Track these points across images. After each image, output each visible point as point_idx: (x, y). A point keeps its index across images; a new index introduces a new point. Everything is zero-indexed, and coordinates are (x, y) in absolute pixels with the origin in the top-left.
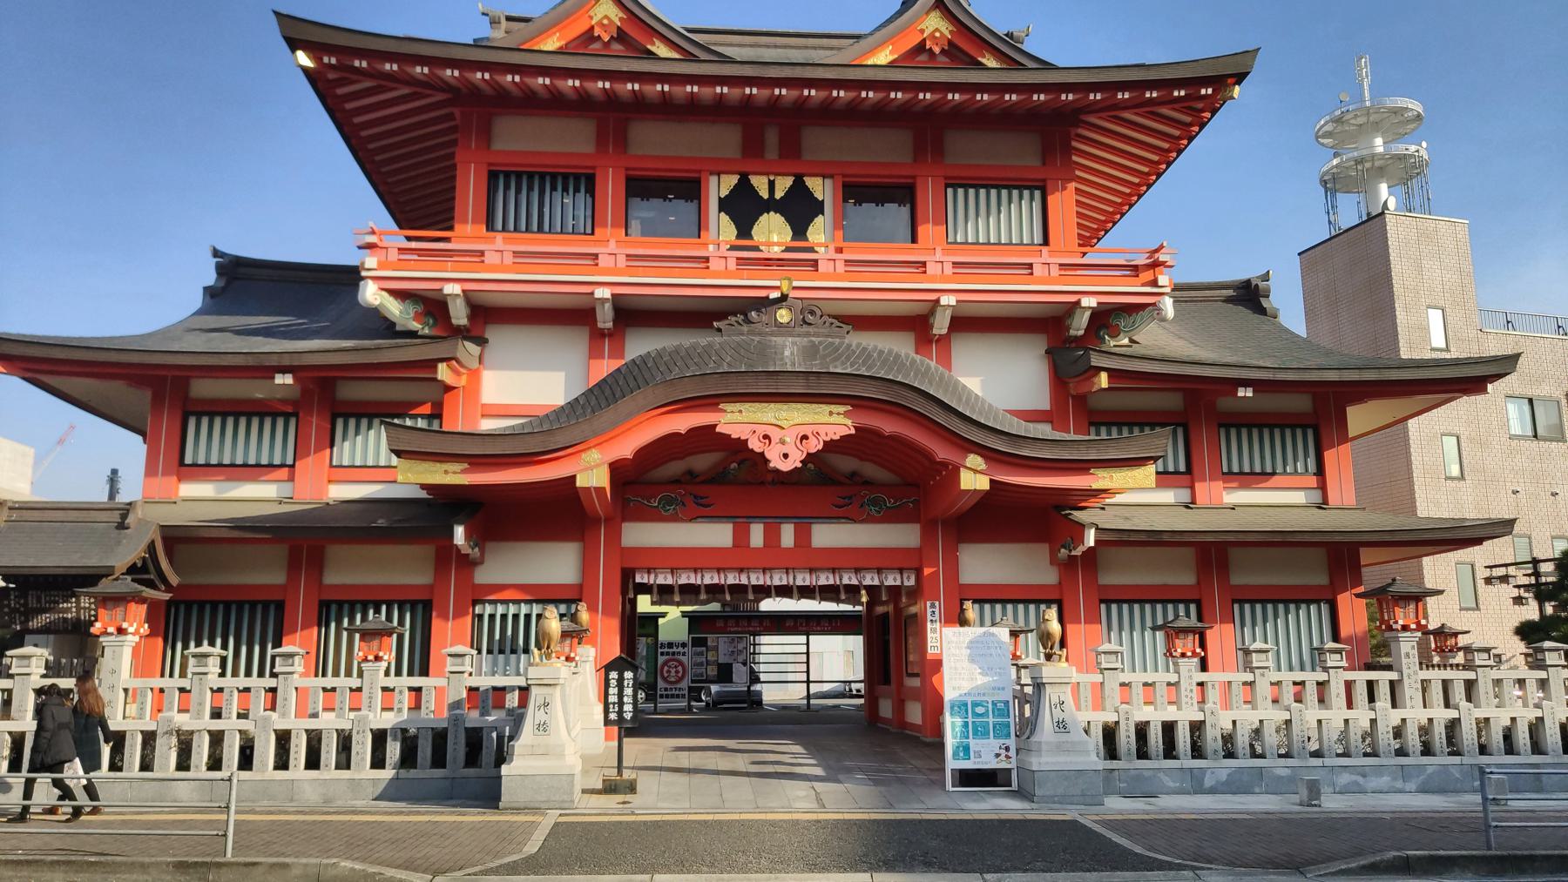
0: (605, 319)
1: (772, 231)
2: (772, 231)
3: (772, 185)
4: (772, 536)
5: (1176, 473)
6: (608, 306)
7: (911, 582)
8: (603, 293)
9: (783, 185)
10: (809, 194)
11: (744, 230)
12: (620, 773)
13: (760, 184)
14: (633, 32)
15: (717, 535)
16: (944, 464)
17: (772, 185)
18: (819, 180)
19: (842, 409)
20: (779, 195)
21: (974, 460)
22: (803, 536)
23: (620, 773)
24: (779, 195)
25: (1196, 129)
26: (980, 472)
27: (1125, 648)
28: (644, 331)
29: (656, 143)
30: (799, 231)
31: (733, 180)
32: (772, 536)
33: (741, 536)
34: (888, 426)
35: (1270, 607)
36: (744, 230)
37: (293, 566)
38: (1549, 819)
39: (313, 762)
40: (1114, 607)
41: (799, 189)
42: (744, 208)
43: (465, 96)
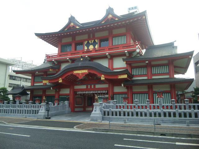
0: (109, 57)
1: (91, 47)
2: (91, 47)
3: (91, 41)
4: (91, 87)
5: (145, 74)
6: (127, 53)
7: (106, 92)
8: (107, 54)
9: (93, 41)
10: (96, 42)
11: (88, 47)
12: (48, 116)
13: (90, 41)
14: (114, 18)
15: (84, 87)
16: (99, 77)
17: (91, 41)
18: (97, 40)
19: (87, 70)
20: (92, 42)
21: (103, 76)
22: (94, 86)
23: (48, 116)
24: (92, 42)
25: (144, 17)
26: (104, 77)
27: (139, 100)
28: (117, 58)
29: (78, 38)
30: (94, 47)
31: (87, 41)
32: (91, 87)
33: (87, 87)
34: (92, 72)
35: (144, 94)
36: (88, 47)
37: (149, 88)
38: (116, 131)
39: (108, 115)
40: (144, 94)
41: (95, 41)
42: (88, 45)
43: (58, 36)
